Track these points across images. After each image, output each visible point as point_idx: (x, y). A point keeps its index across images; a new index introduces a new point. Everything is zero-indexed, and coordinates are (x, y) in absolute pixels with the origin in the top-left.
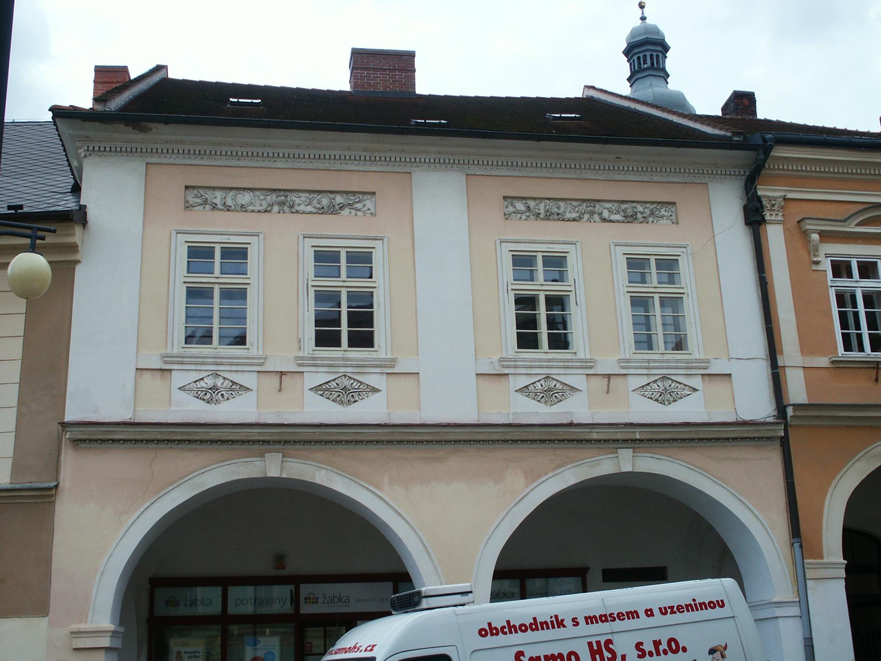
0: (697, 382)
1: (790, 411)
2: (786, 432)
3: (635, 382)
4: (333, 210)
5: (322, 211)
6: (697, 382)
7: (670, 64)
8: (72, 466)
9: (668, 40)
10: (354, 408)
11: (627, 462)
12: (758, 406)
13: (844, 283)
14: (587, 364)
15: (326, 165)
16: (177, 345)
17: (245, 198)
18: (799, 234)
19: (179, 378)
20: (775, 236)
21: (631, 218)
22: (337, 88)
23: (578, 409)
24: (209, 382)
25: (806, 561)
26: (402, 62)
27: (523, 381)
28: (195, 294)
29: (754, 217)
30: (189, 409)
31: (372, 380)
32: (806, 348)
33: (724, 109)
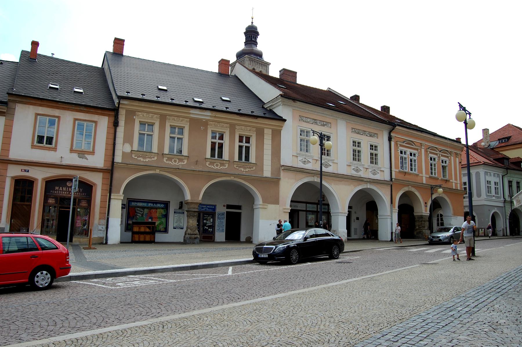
0: (379, 172)
1: (393, 180)
2: (391, 184)
3: (370, 170)
4: (324, 125)
5: (322, 125)
6: (379, 172)
7: (258, 40)
8: (283, 175)
9: (259, 30)
10: (307, 165)
11: (232, 178)
12: (388, 178)
13: (401, 155)
14: (363, 165)
15: (323, 115)
16: (299, 151)
17: (309, 120)
18: (396, 144)
19: (300, 158)
20: (393, 143)
21: (371, 136)
22: (274, 76)
23: (362, 174)
24: (304, 160)
25: (340, 211)
26: (294, 74)
27: (354, 167)
28: (301, 140)
29: (390, 139)
30: (301, 165)
31: (330, 163)
32: (395, 168)
33: (351, 97)
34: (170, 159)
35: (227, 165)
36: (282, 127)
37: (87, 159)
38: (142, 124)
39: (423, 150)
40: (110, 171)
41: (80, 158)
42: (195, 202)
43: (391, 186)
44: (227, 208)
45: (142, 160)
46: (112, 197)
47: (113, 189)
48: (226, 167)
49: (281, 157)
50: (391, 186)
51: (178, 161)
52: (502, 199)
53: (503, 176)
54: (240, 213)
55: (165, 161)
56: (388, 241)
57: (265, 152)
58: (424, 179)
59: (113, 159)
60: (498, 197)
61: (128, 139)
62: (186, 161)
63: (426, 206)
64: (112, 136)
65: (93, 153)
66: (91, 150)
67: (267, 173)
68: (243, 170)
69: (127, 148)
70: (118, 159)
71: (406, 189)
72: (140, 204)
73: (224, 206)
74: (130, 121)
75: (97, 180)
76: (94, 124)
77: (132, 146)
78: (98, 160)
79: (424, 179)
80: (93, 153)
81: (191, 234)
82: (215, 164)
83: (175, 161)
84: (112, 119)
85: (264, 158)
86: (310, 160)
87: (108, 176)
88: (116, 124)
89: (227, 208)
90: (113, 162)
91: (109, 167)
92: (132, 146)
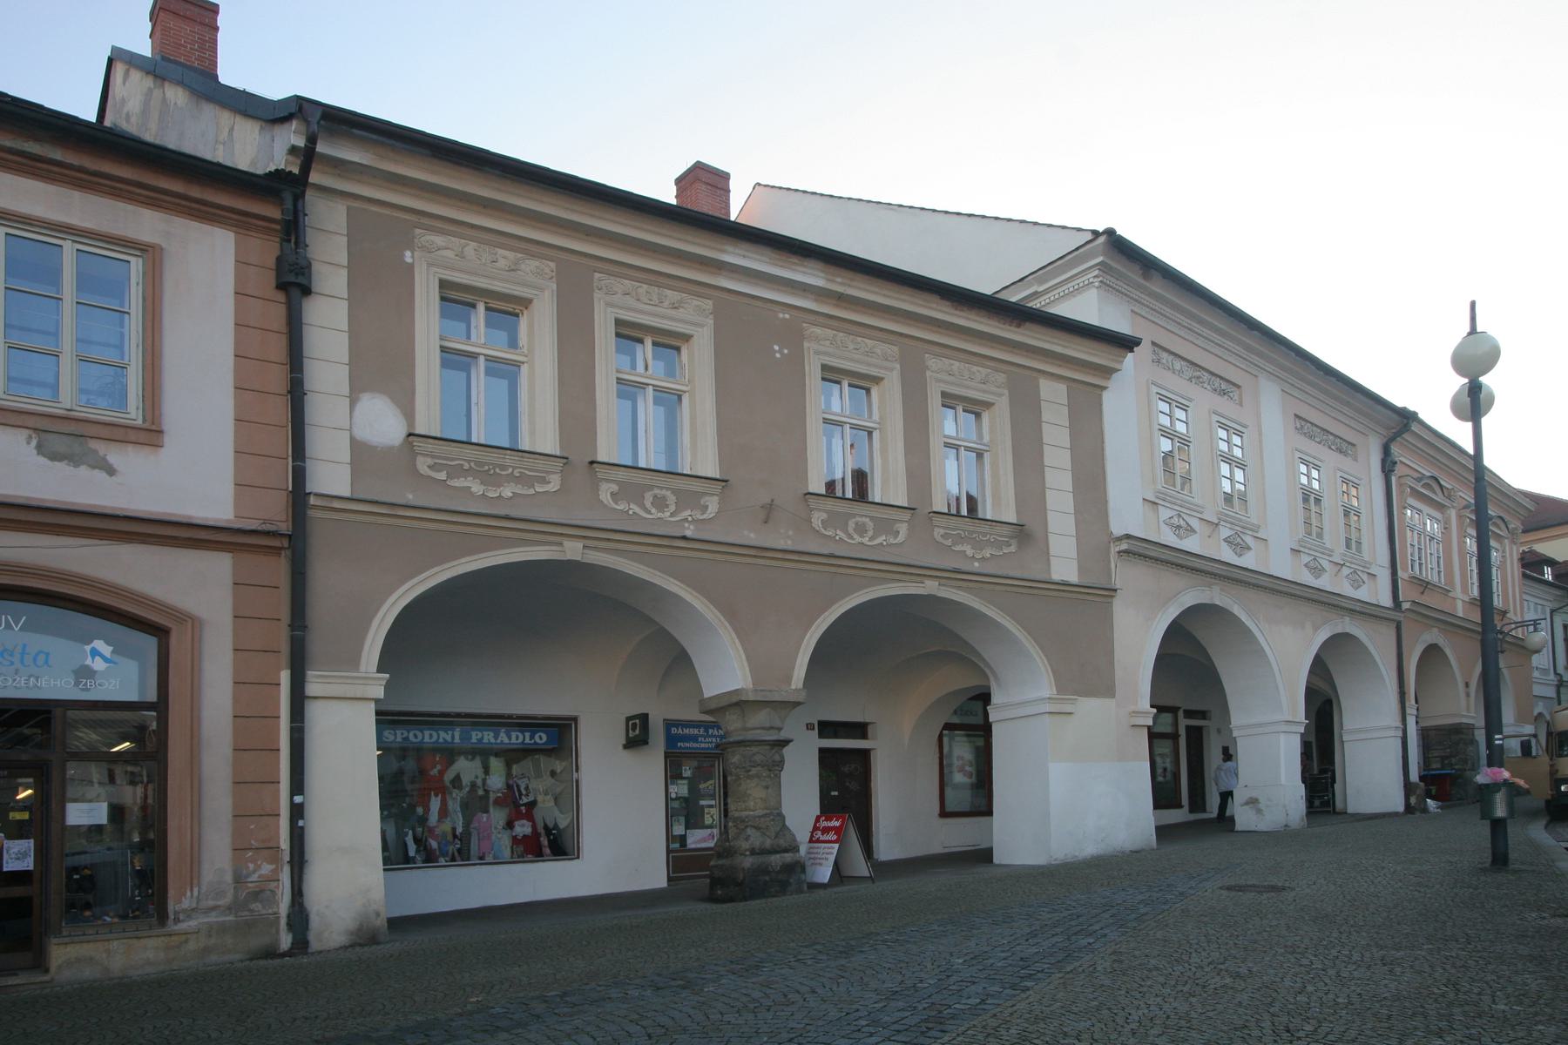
1: (1406, 606)
19: (1165, 513)
29: (1388, 466)
34: (629, 492)
35: (903, 529)
36: (1108, 372)
37: (111, 471)
38: (456, 298)
39: (1453, 513)
40: (283, 541)
41: (54, 457)
42: (777, 698)
43: (1398, 629)
44: (821, 735)
45: (477, 488)
46: (312, 688)
47: (317, 643)
48: (901, 538)
49: (1111, 505)
50: (1398, 629)
51: (671, 499)
52: (1552, 676)
53: (1552, 612)
54: (865, 755)
55: (605, 497)
56: (1396, 814)
57: (1051, 478)
58: (1460, 605)
59: (299, 475)
60: (1545, 672)
61: (379, 366)
62: (713, 504)
63: (1468, 695)
64: (277, 348)
65: (150, 434)
66: (134, 412)
67: (1064, 566)
68: (970, 552)
69: (381, 422)
70: (330, 475)
71: (1433, 636)
72: (454, 736)
73: (810, 727)
74: (381, 285)
75: (201, 588)
76: (136, 265)
77: (409, 414)
78: (196, 469)
79: (1460, 605)
80: (150, 434)
81: (764, 852)
82: (851, 524)
83: (660, 503)
84: (266, 250)
85: (1049, 505)
86: (1195, 523)
87: (277, 571)
88: (294, 282)
89: (821, 735)
90: (299, 496)
91: (273, 511)
92: (409, 414)
